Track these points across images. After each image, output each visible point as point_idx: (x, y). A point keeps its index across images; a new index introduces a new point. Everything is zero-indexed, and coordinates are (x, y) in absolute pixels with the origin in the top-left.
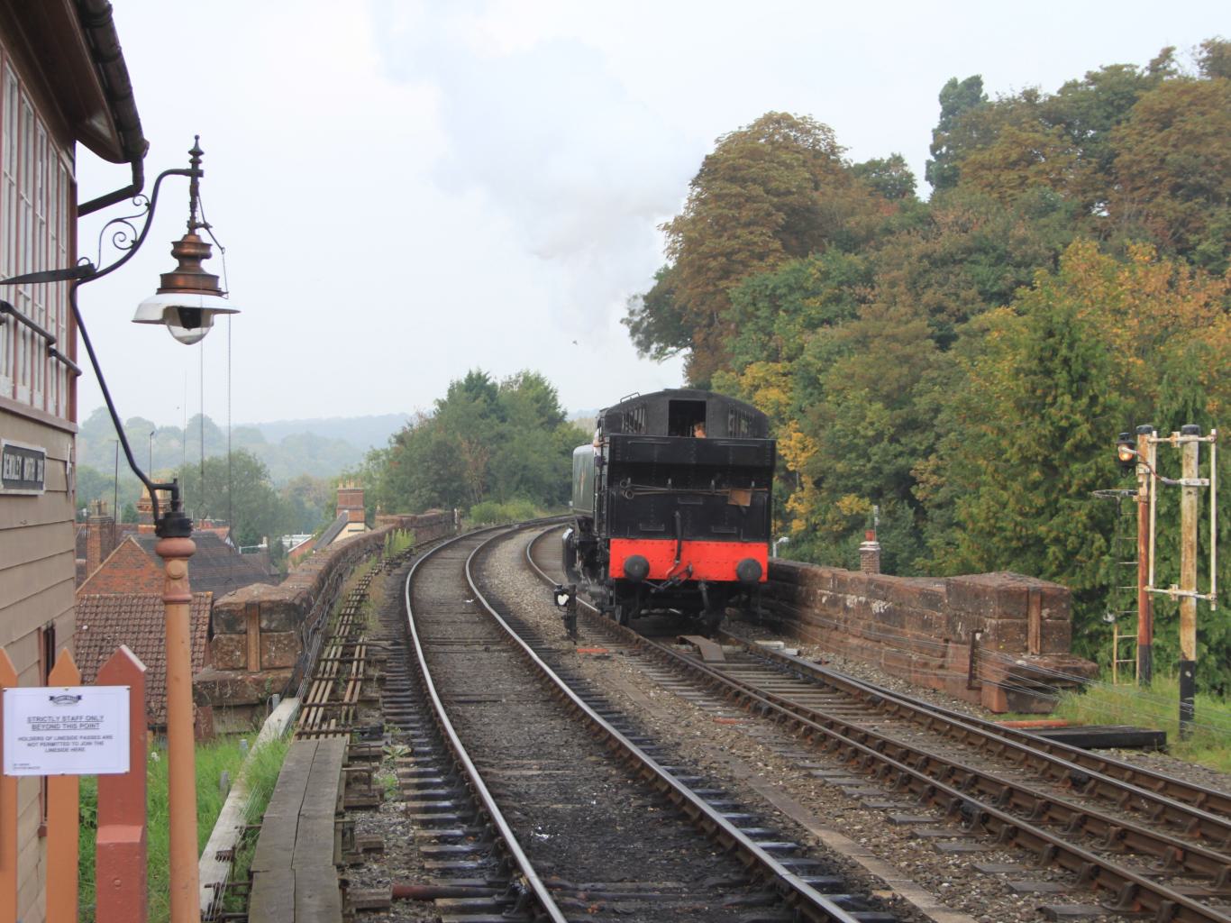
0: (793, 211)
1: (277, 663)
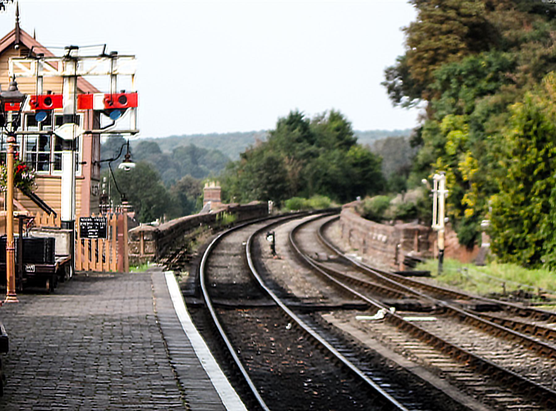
0: (472, 26)
1: (150, 252)
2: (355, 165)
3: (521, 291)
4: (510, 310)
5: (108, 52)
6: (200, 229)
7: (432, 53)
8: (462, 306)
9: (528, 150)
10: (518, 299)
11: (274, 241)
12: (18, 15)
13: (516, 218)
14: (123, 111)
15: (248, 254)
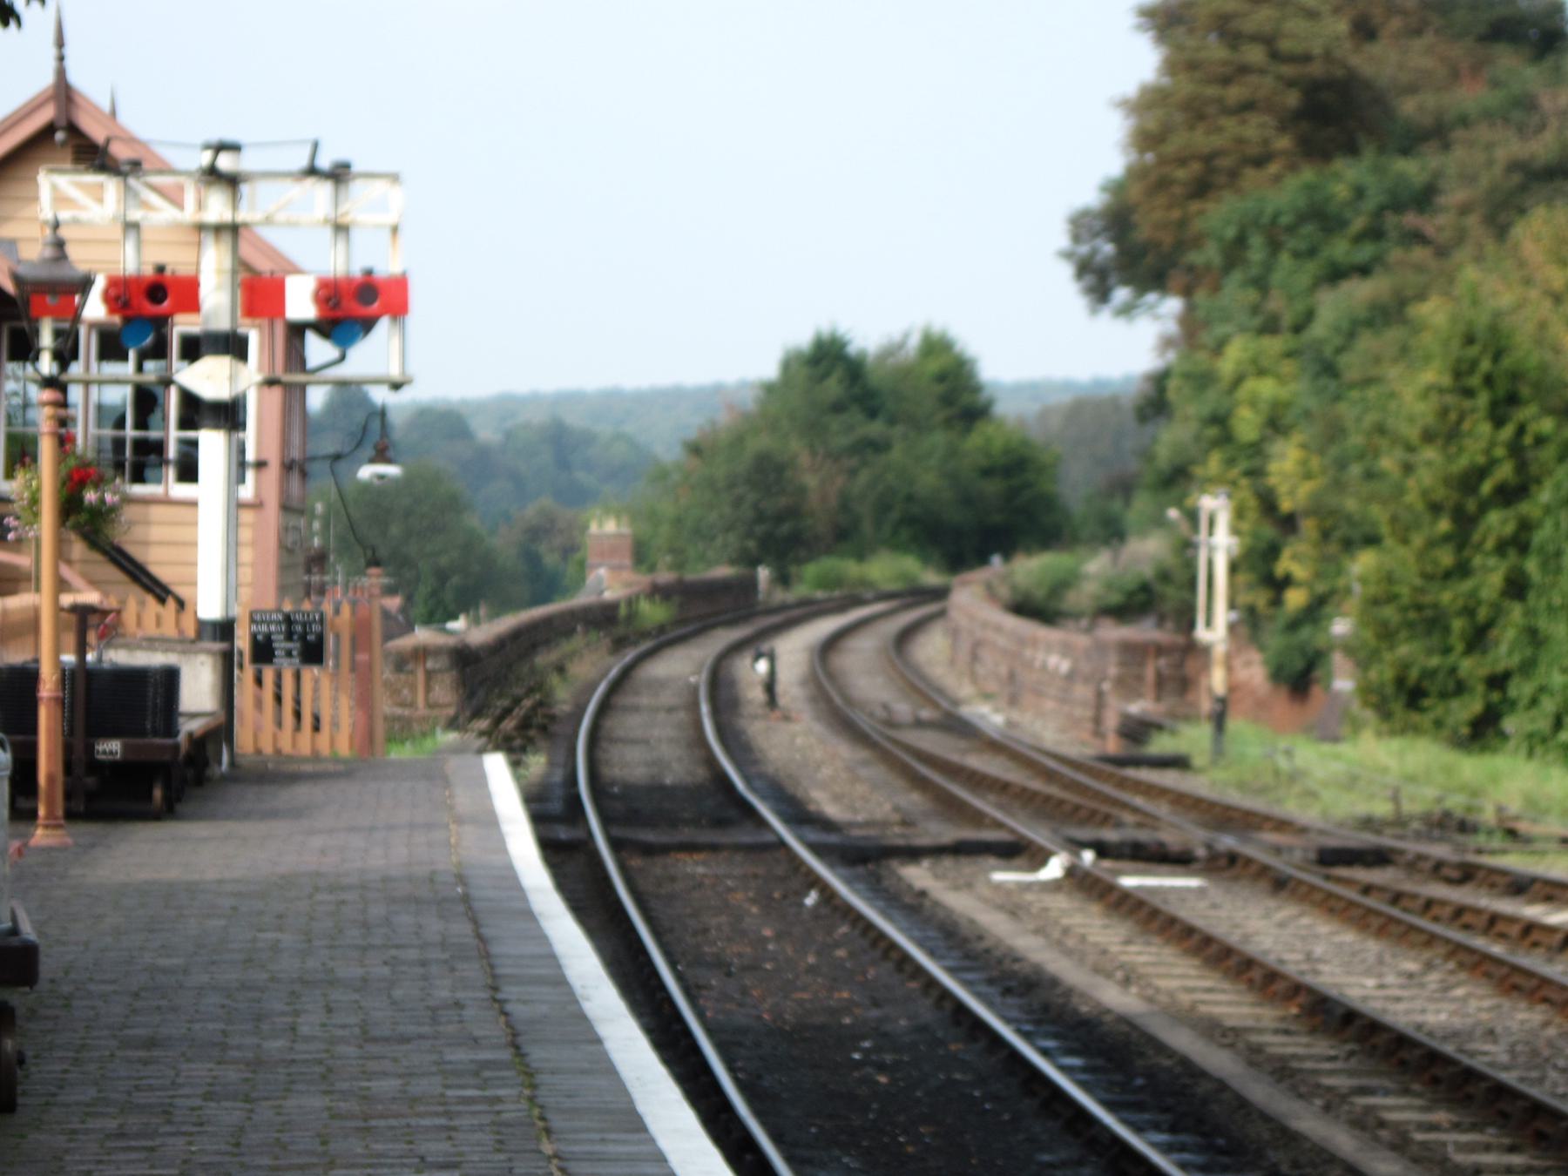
0: (1312, 89)
2: (987, 472)
3: (1447, 815)
4: (1414, 865)
5: (324, 162)
6: (578, 641)
7: (1196, 167)
8: (1278, 850)
9: (1466, 426)
10: (1436, 833)
11: (772, 673)
12: (60, 43)
13: (1429, 613)
14: (368, 325)
15: (705, 708)
